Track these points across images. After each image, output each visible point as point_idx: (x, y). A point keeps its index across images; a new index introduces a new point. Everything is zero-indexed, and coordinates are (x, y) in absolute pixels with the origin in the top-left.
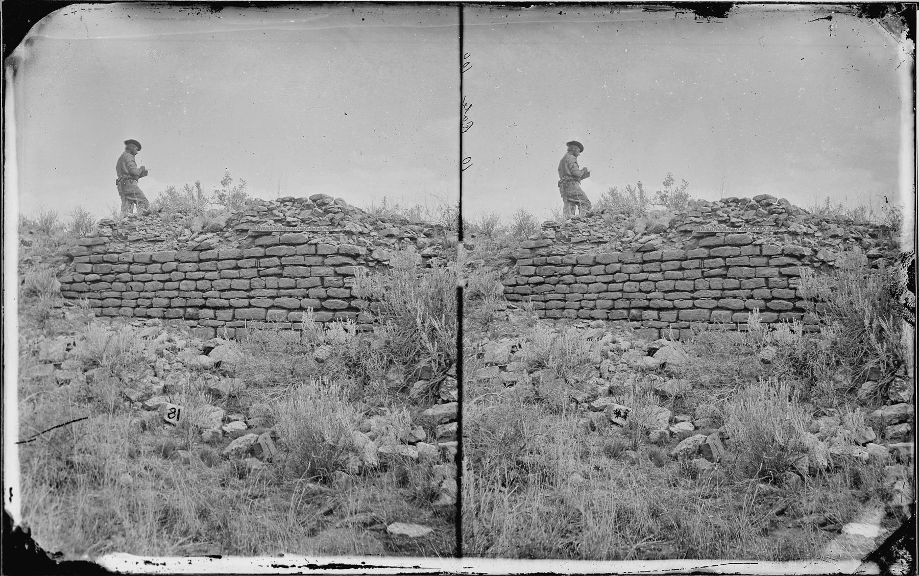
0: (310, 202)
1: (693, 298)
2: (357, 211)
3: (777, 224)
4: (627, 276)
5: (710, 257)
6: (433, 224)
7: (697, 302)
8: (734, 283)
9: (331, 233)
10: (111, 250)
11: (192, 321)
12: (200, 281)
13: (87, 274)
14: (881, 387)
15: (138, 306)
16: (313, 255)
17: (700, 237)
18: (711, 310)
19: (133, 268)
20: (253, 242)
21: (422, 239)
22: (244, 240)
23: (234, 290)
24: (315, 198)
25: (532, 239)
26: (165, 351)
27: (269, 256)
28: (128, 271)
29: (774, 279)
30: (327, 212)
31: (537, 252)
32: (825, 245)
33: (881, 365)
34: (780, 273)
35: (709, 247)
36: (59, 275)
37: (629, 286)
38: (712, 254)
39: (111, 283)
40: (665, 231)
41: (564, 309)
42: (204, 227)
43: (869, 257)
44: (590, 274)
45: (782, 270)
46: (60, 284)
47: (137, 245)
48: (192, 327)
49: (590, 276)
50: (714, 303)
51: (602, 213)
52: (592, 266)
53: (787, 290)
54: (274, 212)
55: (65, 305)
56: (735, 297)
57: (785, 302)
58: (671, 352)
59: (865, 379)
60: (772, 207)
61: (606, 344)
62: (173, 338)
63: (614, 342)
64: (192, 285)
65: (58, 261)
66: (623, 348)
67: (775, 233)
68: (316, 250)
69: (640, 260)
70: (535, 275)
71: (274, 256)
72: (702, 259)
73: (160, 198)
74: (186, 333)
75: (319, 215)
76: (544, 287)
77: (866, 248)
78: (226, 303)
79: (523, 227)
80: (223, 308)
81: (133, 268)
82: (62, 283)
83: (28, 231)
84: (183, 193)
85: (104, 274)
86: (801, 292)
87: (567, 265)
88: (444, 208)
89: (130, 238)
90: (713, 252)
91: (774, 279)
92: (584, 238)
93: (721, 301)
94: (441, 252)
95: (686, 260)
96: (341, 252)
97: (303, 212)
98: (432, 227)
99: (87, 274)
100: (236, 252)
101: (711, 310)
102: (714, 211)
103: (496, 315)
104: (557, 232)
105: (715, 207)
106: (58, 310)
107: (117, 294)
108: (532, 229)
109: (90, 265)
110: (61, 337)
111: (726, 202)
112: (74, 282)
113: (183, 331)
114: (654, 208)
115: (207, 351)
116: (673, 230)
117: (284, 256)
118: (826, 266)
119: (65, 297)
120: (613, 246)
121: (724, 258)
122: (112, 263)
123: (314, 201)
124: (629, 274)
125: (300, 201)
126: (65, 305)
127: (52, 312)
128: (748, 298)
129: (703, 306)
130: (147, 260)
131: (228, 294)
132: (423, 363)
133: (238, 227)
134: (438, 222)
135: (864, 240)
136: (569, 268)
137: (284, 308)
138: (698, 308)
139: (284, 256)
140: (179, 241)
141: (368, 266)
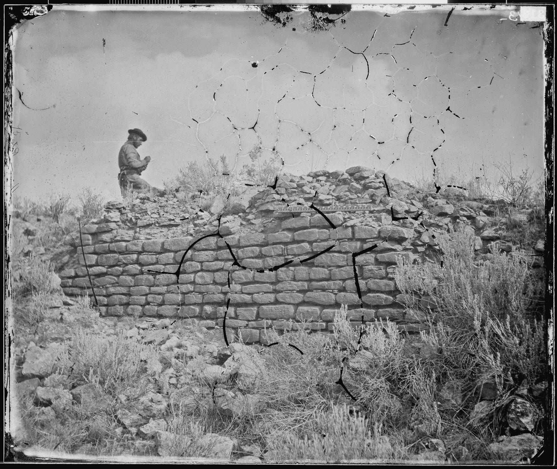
0: (346, 176)
1: (275, 292)
2: (404, 186)
3: (374, 202)
4: (199, 265)
5: (294, 242)
6: (495, 199)
7: (280, 296)
8: (323, 272)
9: (371, 212)
10: (118, 238)
11: (209, 322)
12: (218, 273)
13: (91, 266)
14: (498, 410)
15: (148, 303)
16: (350, 240)
17: (283, 217)
18: (297, 305)
19: (144, 258)
20: (279, 225)
21: (482, 219)
22: (270, 223)
23: (258, 282)
24: (352, 172)
25: (93, 223)
26: (174, 361)
27: (299, 242)
28: (137, 262)
29: (370, 267)
30: (366, 187)
31: (100, 238)
32: (431, 225)
33: (497, 380)
34: (376, 260)
35: (292, 230)
36: (59, 269)
37: (202, 277)
38: (296, 238)
39: (118, 276)
40: (244, 212)
41: (128, 304)
42: (225, 207)
43: (483, 239)
44: (157, 263)
45: (379, 256)
46: (59, 280)
47: (148, 231)
48: (209, 328)
49: (157, 266)
50: (300, 297)
51: (177, 191)
52: (160, 253)
53: (385, 281)
54: (305, 188)
55: (65, 304)
56: (324, 290)
57: (384, 296)
58: (248, 361)
59: (479, 397)
60: (367, 181)
61: (170, 349)
62: (183, 343)
63: (179, 346)
64: (208, 277)
65: (61, 253)
66: (189, 353)
67: (371, 212)
68: (353, 233)
69: (213, 246)
70: (97, 265)
71: (303, 241)
72: (286, 244)
73: (180, 175)
74: (201, 336)
75: (357, 192)
76: (107, 278)
77: (478, 230)
78: (247, 298)
79: (90, 209)
80: (245, 304)
81: (144, 258)
82: (62, 278)
83: (36, 218)
84: (206, 170)
85: (111, 266)
86: (400, 282)
87: (133, 252)
88: (507, 180)
89: (140, 223)
90: (297, 235)
91: (370, 267)
92: (153, 221)
93: (309, 294)
94: (504, 234)
95: (267, 245)
96: (382, 235)
97: (339, 188)
98: (493, 202)
99: (91, 266)
100: (260, 238)
101: (297, 305)
102: (300, 186)
103: (48, 313)
104: (122, 214)
105: (302, 182)
106: (56, 310)
107: (124, 290)
108: (95, 212)
109: (95, 257)
110: (54, 344)
111: (316, 176)
112: (77, 276)
113: (198, 334)
114: (237, 182)
115: (221, 360)
116: (254, 211)
117: (316, 241)
118: (432, 251)
119: (67, 294)
120: (184, 229)
121: (311, 243)
122: (120, 253)
123: (351, 175)
124: (201, 262)
125: (335, 175)
126: (65, 304)
127: (48, 313)
128: (340, 291)
129: (288, 300)
130: (158, 249)
131: (250, 288)
132: (485, 378)
133: (264, 208)
134: (501, 197)
135: (478, 218)
136: (135, 256)
137: (316, 305)
138: (281, 303)
139: (316, 241)
140: (196, 225)
141: (415, 251)
